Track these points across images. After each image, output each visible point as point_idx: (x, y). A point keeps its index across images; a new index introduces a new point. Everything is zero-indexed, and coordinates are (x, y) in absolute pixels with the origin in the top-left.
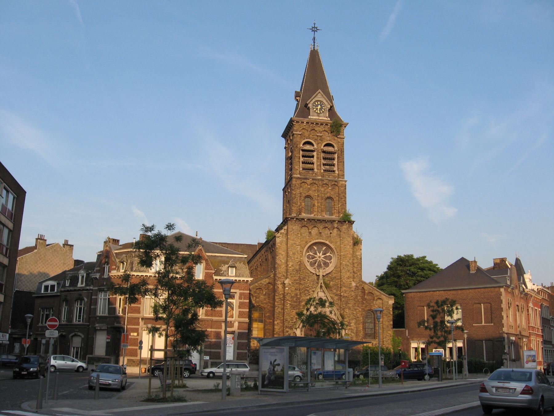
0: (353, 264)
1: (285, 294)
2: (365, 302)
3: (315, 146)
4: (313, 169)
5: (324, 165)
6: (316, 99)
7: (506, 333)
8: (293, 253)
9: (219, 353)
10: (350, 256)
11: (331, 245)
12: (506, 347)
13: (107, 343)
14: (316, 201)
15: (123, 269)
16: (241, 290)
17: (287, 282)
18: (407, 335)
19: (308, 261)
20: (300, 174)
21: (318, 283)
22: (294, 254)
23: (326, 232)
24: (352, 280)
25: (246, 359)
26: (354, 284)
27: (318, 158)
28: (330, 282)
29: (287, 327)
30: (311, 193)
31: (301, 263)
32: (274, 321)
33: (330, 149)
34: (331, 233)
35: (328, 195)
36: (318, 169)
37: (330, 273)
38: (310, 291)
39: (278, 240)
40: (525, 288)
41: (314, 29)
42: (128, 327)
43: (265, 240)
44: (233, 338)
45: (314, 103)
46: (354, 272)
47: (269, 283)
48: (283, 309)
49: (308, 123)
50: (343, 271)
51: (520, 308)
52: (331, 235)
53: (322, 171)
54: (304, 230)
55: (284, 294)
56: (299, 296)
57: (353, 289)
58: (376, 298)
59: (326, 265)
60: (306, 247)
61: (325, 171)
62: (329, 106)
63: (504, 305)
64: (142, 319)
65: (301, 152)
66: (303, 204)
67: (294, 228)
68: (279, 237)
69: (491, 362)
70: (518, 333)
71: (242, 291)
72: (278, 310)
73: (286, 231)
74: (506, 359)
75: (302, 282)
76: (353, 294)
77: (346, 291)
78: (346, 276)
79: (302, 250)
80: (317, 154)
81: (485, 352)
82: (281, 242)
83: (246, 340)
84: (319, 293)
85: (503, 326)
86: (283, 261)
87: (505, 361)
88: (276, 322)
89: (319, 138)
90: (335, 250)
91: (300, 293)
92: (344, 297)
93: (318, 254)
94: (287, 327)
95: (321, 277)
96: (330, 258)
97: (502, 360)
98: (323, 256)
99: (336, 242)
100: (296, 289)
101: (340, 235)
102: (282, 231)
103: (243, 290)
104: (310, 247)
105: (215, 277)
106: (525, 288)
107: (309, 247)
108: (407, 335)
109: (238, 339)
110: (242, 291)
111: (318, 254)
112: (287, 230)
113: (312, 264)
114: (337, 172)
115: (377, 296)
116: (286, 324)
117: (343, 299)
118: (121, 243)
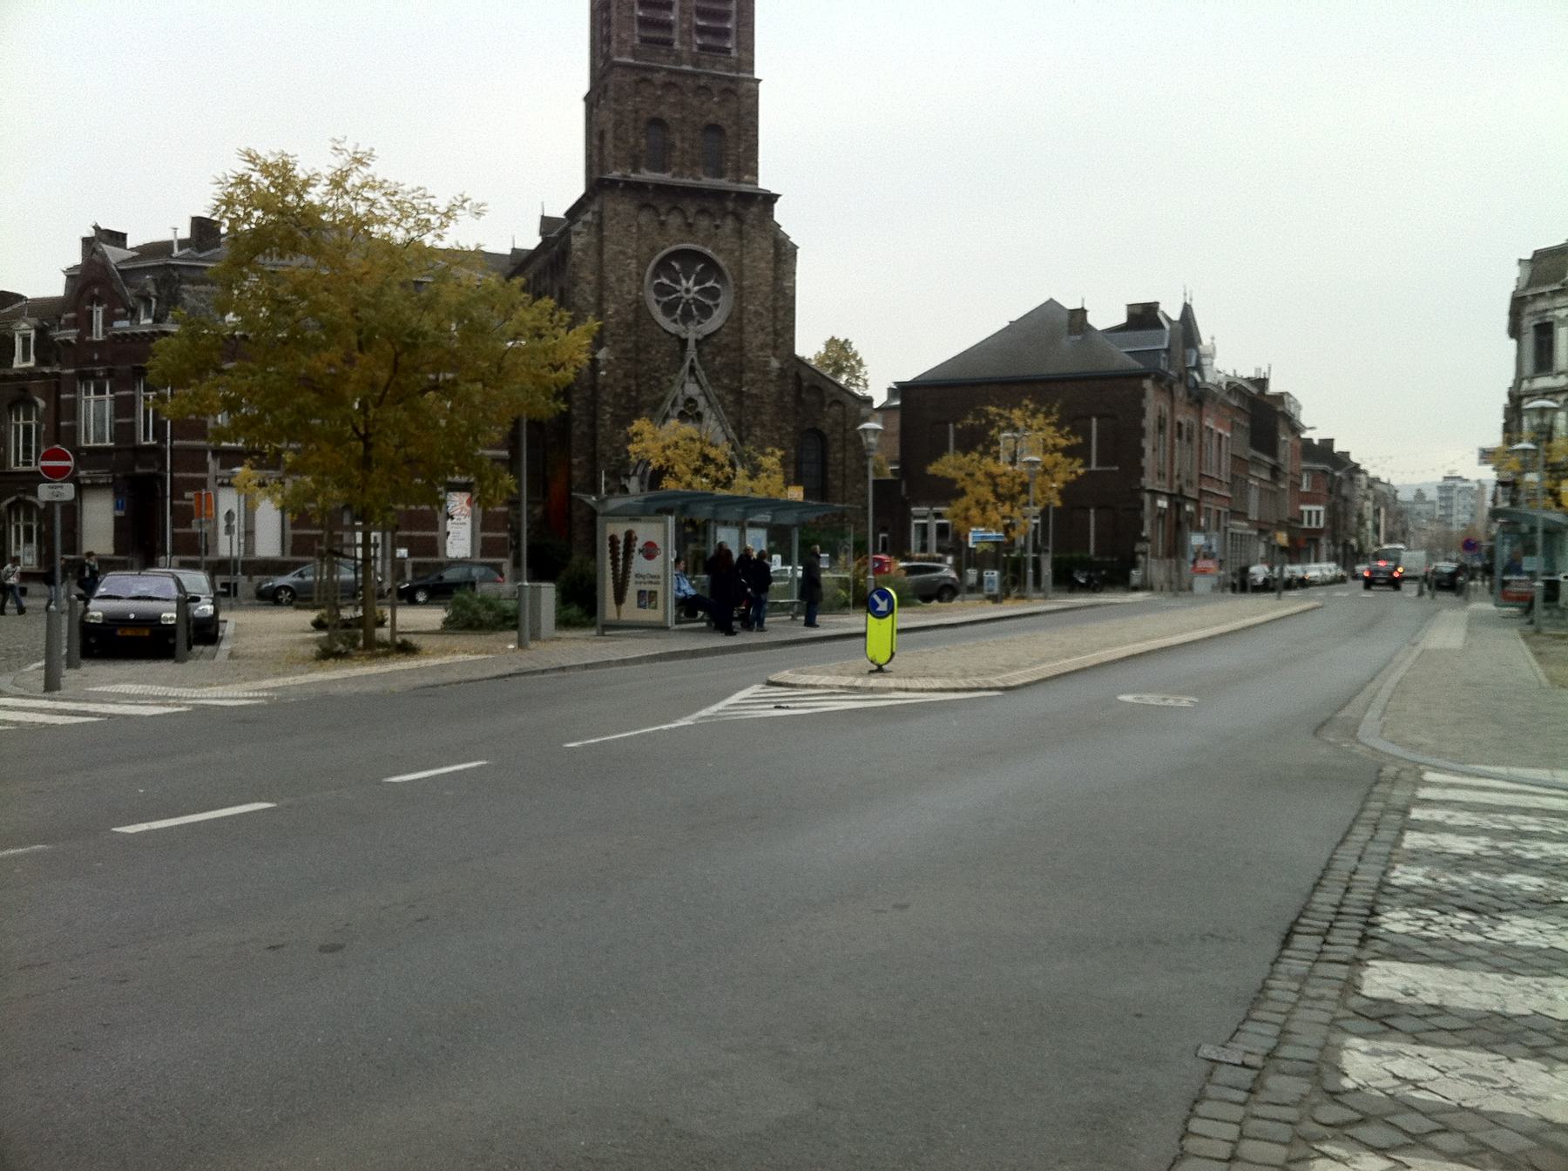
9: (433, 540)
11: (720, 260)
21: (682, 360)
22: (620, 280)
24: (769, 352)
25: (505, 555)
30: (665, 111)
31: (640, 308)
34: (717, 227)
35: (711, 118)
36: (682, 43)
48: (593, 425)
50: (749, 329)
54: (644, 217)
57: (773, 376)
58: (828, 400)
59: (706, 312)
61: (702, 48)
68: (578, 234)
75: (643, 356)
77: (753, 382)
78: (757, 342)
86: (592, 300)
88: (575, 461)
92: (750, 396)
95: (691, 344)
96: (713, 294)
99: (732, 252)
100: (626, 376)
104: (664, 266)
113: (669, 309)
114: (734, 53)
115: (832, 395)
117: (747, 402)
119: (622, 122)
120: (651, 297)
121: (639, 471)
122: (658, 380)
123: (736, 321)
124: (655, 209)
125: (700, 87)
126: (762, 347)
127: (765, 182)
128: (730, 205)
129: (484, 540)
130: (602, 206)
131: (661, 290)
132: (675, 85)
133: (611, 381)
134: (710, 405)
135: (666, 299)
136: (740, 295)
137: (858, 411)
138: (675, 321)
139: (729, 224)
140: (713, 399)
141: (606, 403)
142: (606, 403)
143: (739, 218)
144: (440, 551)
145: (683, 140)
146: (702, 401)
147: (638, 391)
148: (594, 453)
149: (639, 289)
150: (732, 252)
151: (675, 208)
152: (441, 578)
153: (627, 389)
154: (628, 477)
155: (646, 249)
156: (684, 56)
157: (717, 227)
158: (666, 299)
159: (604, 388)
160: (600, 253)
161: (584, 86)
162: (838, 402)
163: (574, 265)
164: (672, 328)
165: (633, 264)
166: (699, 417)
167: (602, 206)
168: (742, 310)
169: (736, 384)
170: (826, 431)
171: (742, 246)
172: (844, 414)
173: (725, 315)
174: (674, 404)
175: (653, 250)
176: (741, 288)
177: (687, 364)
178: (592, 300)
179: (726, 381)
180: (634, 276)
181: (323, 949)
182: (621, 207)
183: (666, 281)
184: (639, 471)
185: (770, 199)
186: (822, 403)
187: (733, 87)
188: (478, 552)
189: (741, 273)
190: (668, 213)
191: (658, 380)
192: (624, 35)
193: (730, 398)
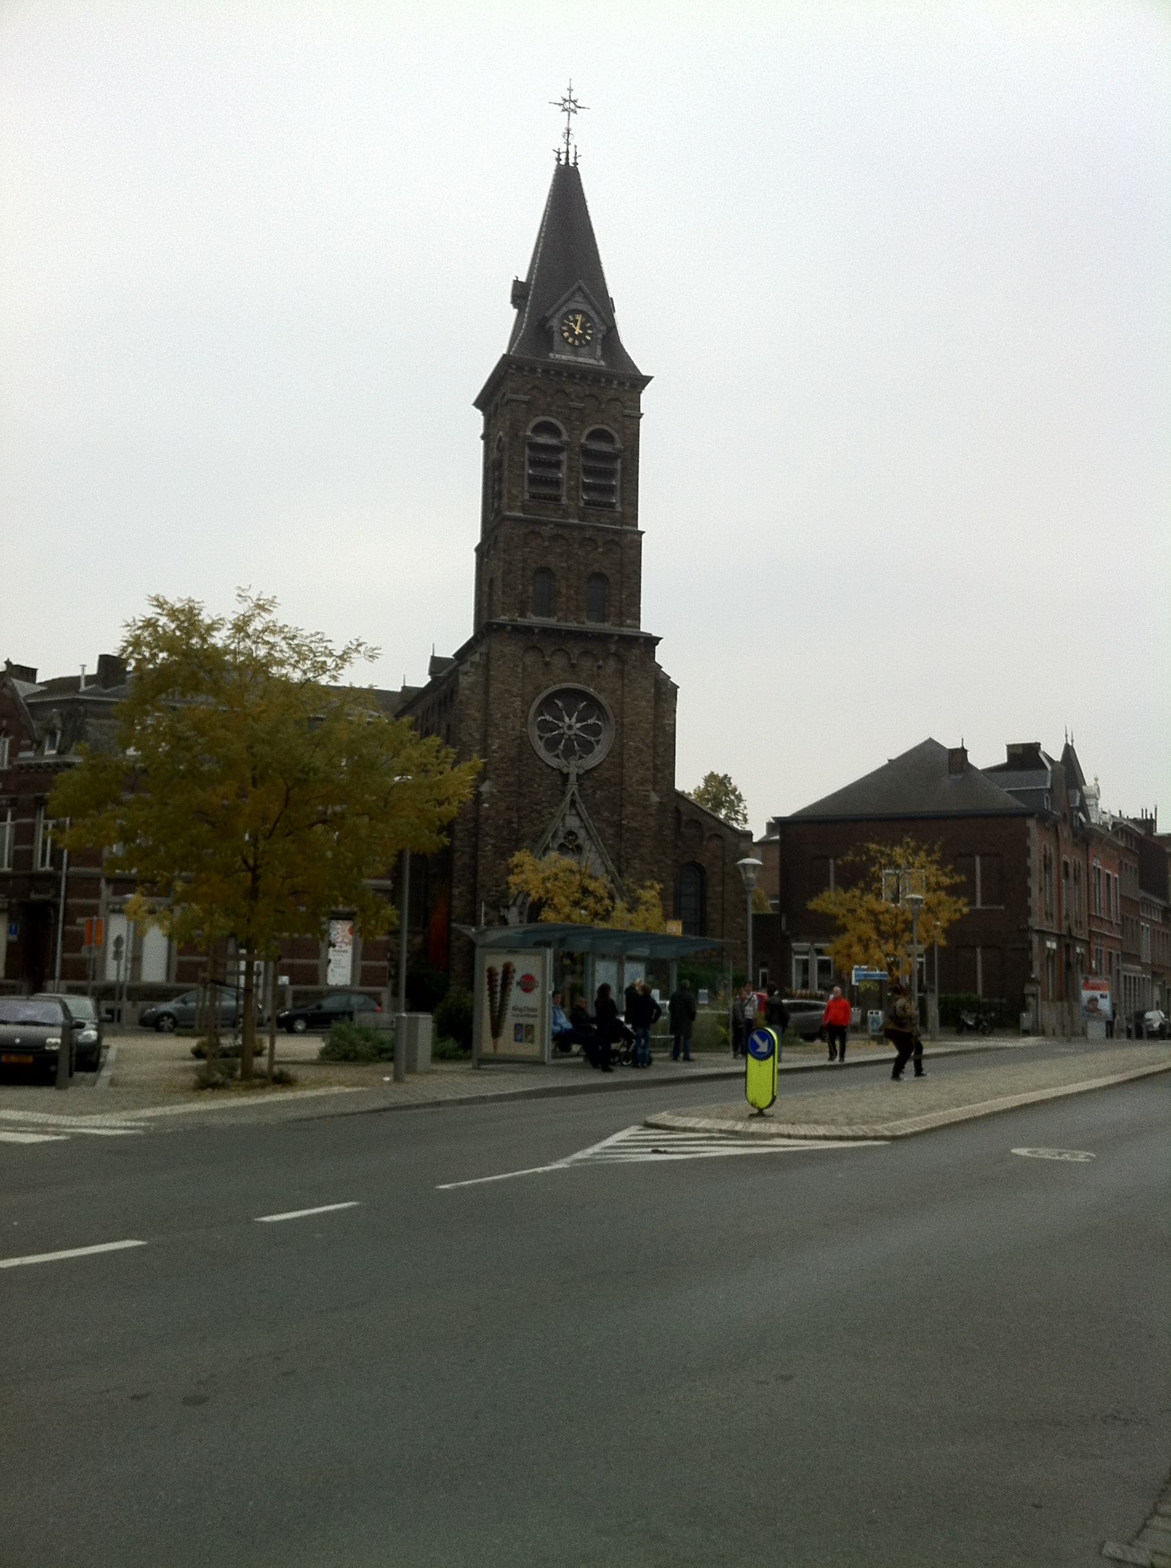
0: (655, 747)
1: (481, 820)
2: (680, 843)
3: (565, 437)
4: (557, 499)
5: (587, 488)
7: (1038, 931)
11: (602, 699)
12: (1036, 965)
13: (10, 945)
15: (52, 747)
18: (783, 927)
19: (541, 738)
20: (524, 509)
21: (563, 793)
22: (505, 717)
25: (384, 985)
26: (655, 798)
27: (570, 468)
28: (594, 793)
31: (523, 743)
33: (604, 447)
35: (596, 568)
36: (569, 499)
37: (594, 769)
38: (545, 812)
39: (464, 681)
40: (1084, 819)
41: (570, 106)
42: (70, 901)
43: (429, 679)
45: (565, 316)
46: (656, 768)
48: (474, 857)
49: (546, 372)
51: (1071, 870)
53: (582, 504)
54: (529, 659)
56: (515, 825)
58: (707, 834)
59: (588, 748)
60: (537, 702)
61: (587, 503)
62: (603, 328)
63: (1035, 861)
64: (108, 881)
65: (527, 451)
66: (531, 589)
68: (466, 673)
69: (997, 1000)
70: (1064, 932)
73: (484, 657)
74: (1034, 995)
76: (652, 823)
80: (570, 458)
81: (980, 976)
85: (1028, 912)
87: (1030, 1000)
88: (456, 891)
90: (610, 712)
91: (520, 818)
93: (567, 719)
96: (595, 730)
97: (1024, 997)
98: (578, 725)
100: (508, 808)
102: (476, 658)
106: (1084, 819)
107: (542, 703)
108: (783, 927)
111: (567, 719)
112: (488, 654)
113: (551, 745)
114: (619, 508)
117: (627, 835)
118: (40, 678)
120: (534, 733)
121: (519, 902)
122: (539, 812)
123: (617, 755)
124: (540, 650)
131: (545, 727)
132: (562, 536)
134: (590, 837)
135: (549, 735)
139: (612, 664)
140: (594, 832)
145: (569, 587)
146: (582, 834)
149: (524, 725)
151: (560, 650)
152: (319, 1007)
154: (507, 907)
157: (599, 667)
158: (549, 735)
159: (487, 819)
161: (478, 540)
164: (554, 762)
165: (518, 702)
166: (579, 849)
169: (616, 818)
171: (623, 685)
174: (554, 837)
175: (538, 689)
176: (622, 725)
177: (568, 798)
179: (606, 814)
180: (519, 714)
183: (548, 718)
184: (519, 902)
185: (653, 641)
187: (617, 539)
190: (553, 654)
191: (539, 812)
192: (514, 492)
193: (610, 831)
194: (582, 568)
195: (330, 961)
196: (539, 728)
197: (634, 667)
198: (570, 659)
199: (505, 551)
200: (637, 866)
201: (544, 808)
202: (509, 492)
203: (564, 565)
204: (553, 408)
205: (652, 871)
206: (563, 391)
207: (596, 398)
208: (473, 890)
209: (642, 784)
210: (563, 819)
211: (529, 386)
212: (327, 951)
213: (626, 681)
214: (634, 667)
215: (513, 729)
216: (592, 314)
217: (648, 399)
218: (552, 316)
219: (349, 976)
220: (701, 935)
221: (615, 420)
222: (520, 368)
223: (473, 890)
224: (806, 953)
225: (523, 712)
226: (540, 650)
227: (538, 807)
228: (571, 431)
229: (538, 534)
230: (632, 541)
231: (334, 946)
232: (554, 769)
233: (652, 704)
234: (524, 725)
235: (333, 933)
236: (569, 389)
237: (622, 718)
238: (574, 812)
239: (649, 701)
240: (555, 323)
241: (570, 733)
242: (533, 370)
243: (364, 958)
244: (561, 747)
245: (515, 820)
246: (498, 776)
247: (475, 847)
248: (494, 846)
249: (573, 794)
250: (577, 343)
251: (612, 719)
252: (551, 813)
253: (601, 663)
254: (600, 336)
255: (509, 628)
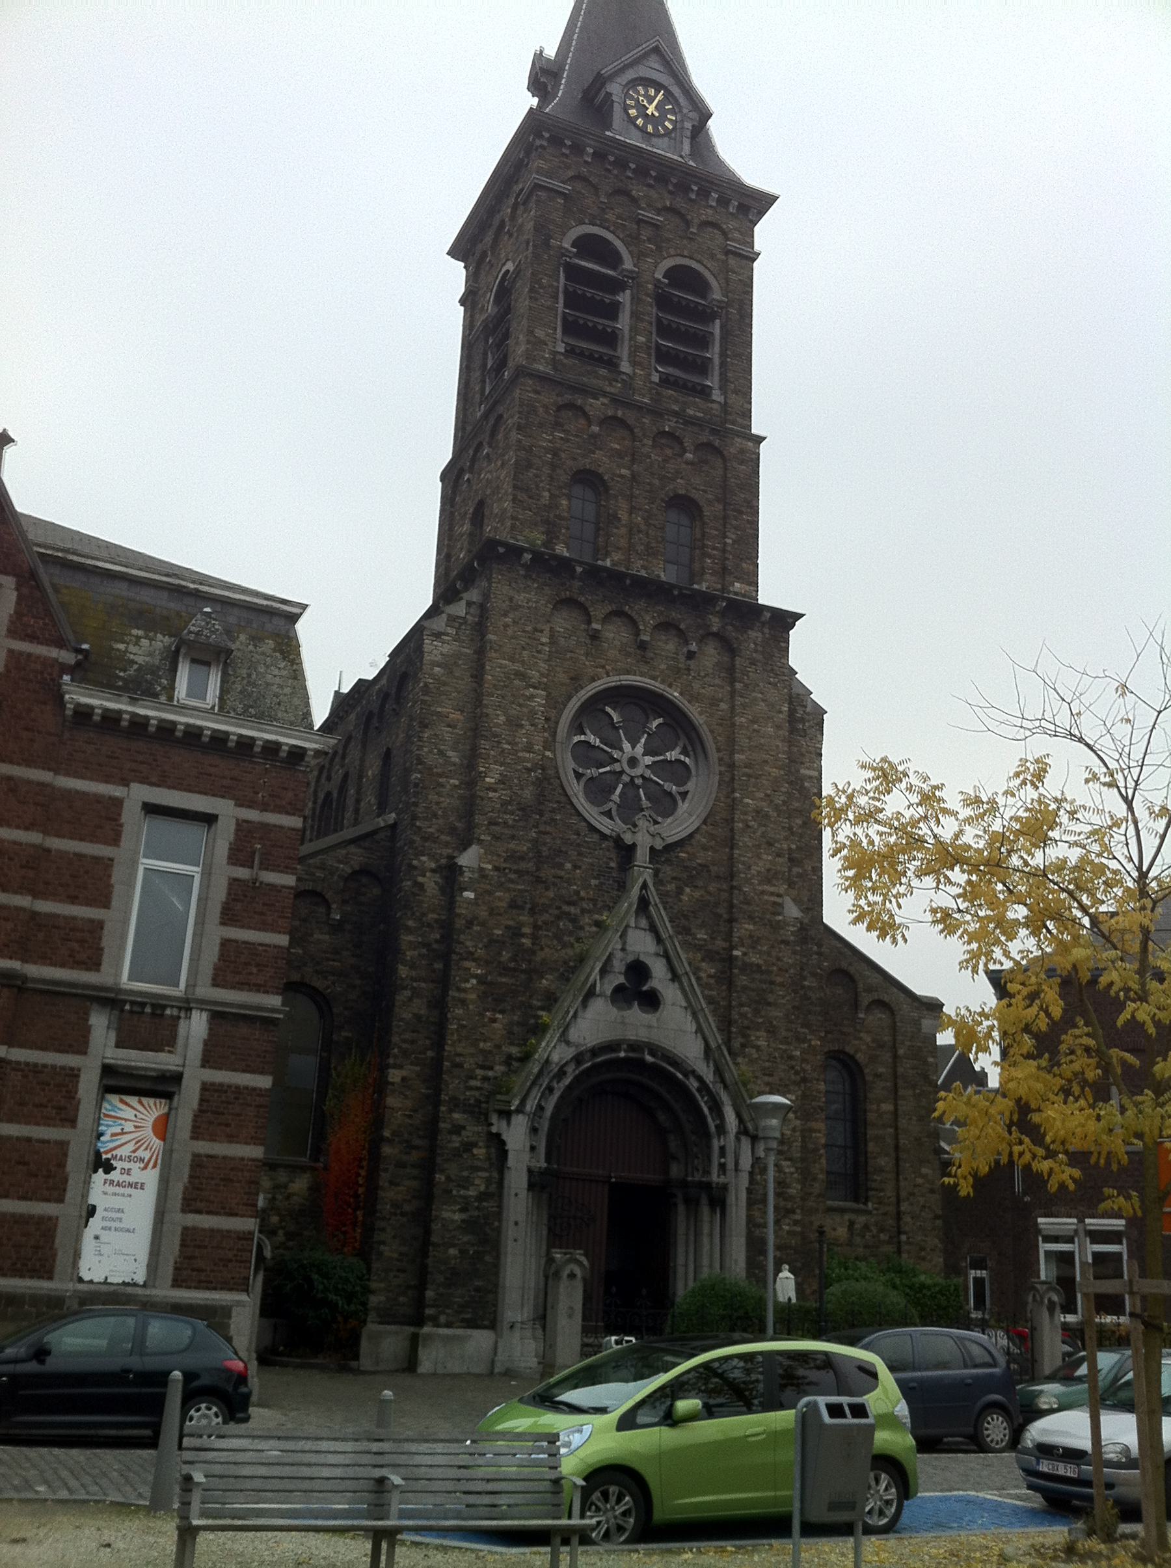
1: (460, 923)
3: (628, 264)
4: (612, 364)
6: (642, 71)
8: (509, 722)
9: (46, 1228)
10: (775, 772)
11: (694, 711)
14: (623, 504)
16: (250, 804)
17: (469, 859)
19: (578, 776)
21: (622, 886)
22: (514, 724)
23: (671, 646)
25: (243, 1286)
28: (680, 891)
29: (455, 1104)
30: (602, 462)
31: (547, 780)
32: (383, 1069)
34: (691, 655)
35: (680, 486)
36: (634, 363)
44: (162, 1128)
47: (363, 871)
48: (439, 1004)
49: (599, 156)
50: (744, 840)
52: (692, 663)
54: (563, 622)
55: (448, 929)
58: (865, 999)
59: (666, 804)
60: (574, 705)
67: (520, 598)
68: (438, 635)
71: (253, 815)
72: (409, 1008)
75: (547, 872)
77: (755, 941)
79: (553, 714)
80: (635, 300)
82: (448, 664)
83: (254, 1140)
84: (632, 935)
86: (454, 757)
88: (395, 1076)
89: (646, 233)
91: (536, 927)
92: (746, 968)
93: (627, 746)
94: (455, 1104)
95: (642, 856)
96: (679, 773)
98: (648, 760)
99: (714, 702)
100: (513, 905)
101: (731, 670)
103: (264, 808)
104: (593, 708)
105: (78, 695)
109: (196, 1134)
110: (253, 815)
111: (627, 746)
113: (598, 790)
114: (717, 395)
115: (869, 989)
116: (453, 1085)
117: (742, 980)
119: (530, 465)
120: (568, 764)
121: (530, 1106)
122: (574, 920)
123: (723, 823)
124: (582, 607)
125: (663, 434)
126: (769, 877)
127: (771, 592)
128: (715, 623)
129: (189, 1237)
130: (486, 596)
131: (584, 752)
132: (622, 422)
133: (483, 913)
134: (675, 977)
135: (591, 772)
136: (729, 783)
137: (917, 1023)
138: (608, 814)
139: (711, 655)
140: (683, 967)
141: (470, 956)
142: (470, 956)
143: (729, 648)
144: (62, 1260)
145: (632, 510)
146: (658, 969)
147: (535, 938)
148: (438, 1062)
149: (549, 745)
150: (714, 702)
151: (619, 613)
152: (41, 1354)
153: (515, 932)
154: (506, 1114)
155: (562, 677)
156: (639, 383)
157: (691, 655)
158: (591, 772)
159: (470, 924)
160: (478, 675)
161: (445, 454)
162: (881, 1004)
163: (426, 690)
164: (605, 825)
165: (539, 700)
166: (651, 1001)
167: (486, 596)
168: (732, 806)
169: (720, 944)
170: (860, 1057)
171: (733, 693)
172: (894, 1028)
173: (701, 811)
174: (604, 972)
175: (576, 681)
176: (732, 766)
177: (635, 892)
178: (454, 757)
179: (702, 935)
180: (541, 722)
181: (481, 504)
182: (516, 597)
184: (530, 1106)
185: (785, 620)
186: (856, 1006)
188: (167, 1270)
189: (731, 741)
190: (606, 619)
191: (574, 920)
192: (540, 333)
193: (709, 969)
194: (656, 482)
195: (92, 1211)
196: (575, 758)
197: (753, 663)
198: (637, 633)
199: (519, 428)
200: (762, 1043)
201: (583, 911)
202: (531, 332)
203: (624, 471)
204: (610, 216)
205: (791, 1058)
206: (626, 193)
207: (682, 216)
208: (435, 1074)
209: (769, 882)
210: (623, 936)
211: (571, 173)
212: (87, 1183)
213: (738, 686)
214: (753, 663)
215: (529, 748)
216: (676, 91)
217: (766, 233)
218: (611, 78)
219: (143, 1255)
220: (856, 1200)
221: (713, 256)
222: (556, 141)
223: (435, 1074)
224: (1070, 1240)
225: (547, 719)
226: (582, 607)
227: (572, 909)
228: (639, 257)
229: (581, 411)
230: (742, 451)
231: (109, 1168)
232: (604, 837)
233: (784, 733)
234: (549, 745)
235: (109, 1129)
236: (638, 191)
237: (732, 753)
238: (644, 923)
239: (778, 727)
240: (615, 89)
241: (638, 771)
242: (578, 149)
243: (189, 1205)
244: (616, 797)
245: (527, 930)
246: (496, 838)
247: (444, 982)
248: (481, 980)
249: (645, 886)
250: (650, 128)
251: (714, 755)
252: (598, 924)
253: (693, 647)
254: (688, 125)
255: (527, 556)
